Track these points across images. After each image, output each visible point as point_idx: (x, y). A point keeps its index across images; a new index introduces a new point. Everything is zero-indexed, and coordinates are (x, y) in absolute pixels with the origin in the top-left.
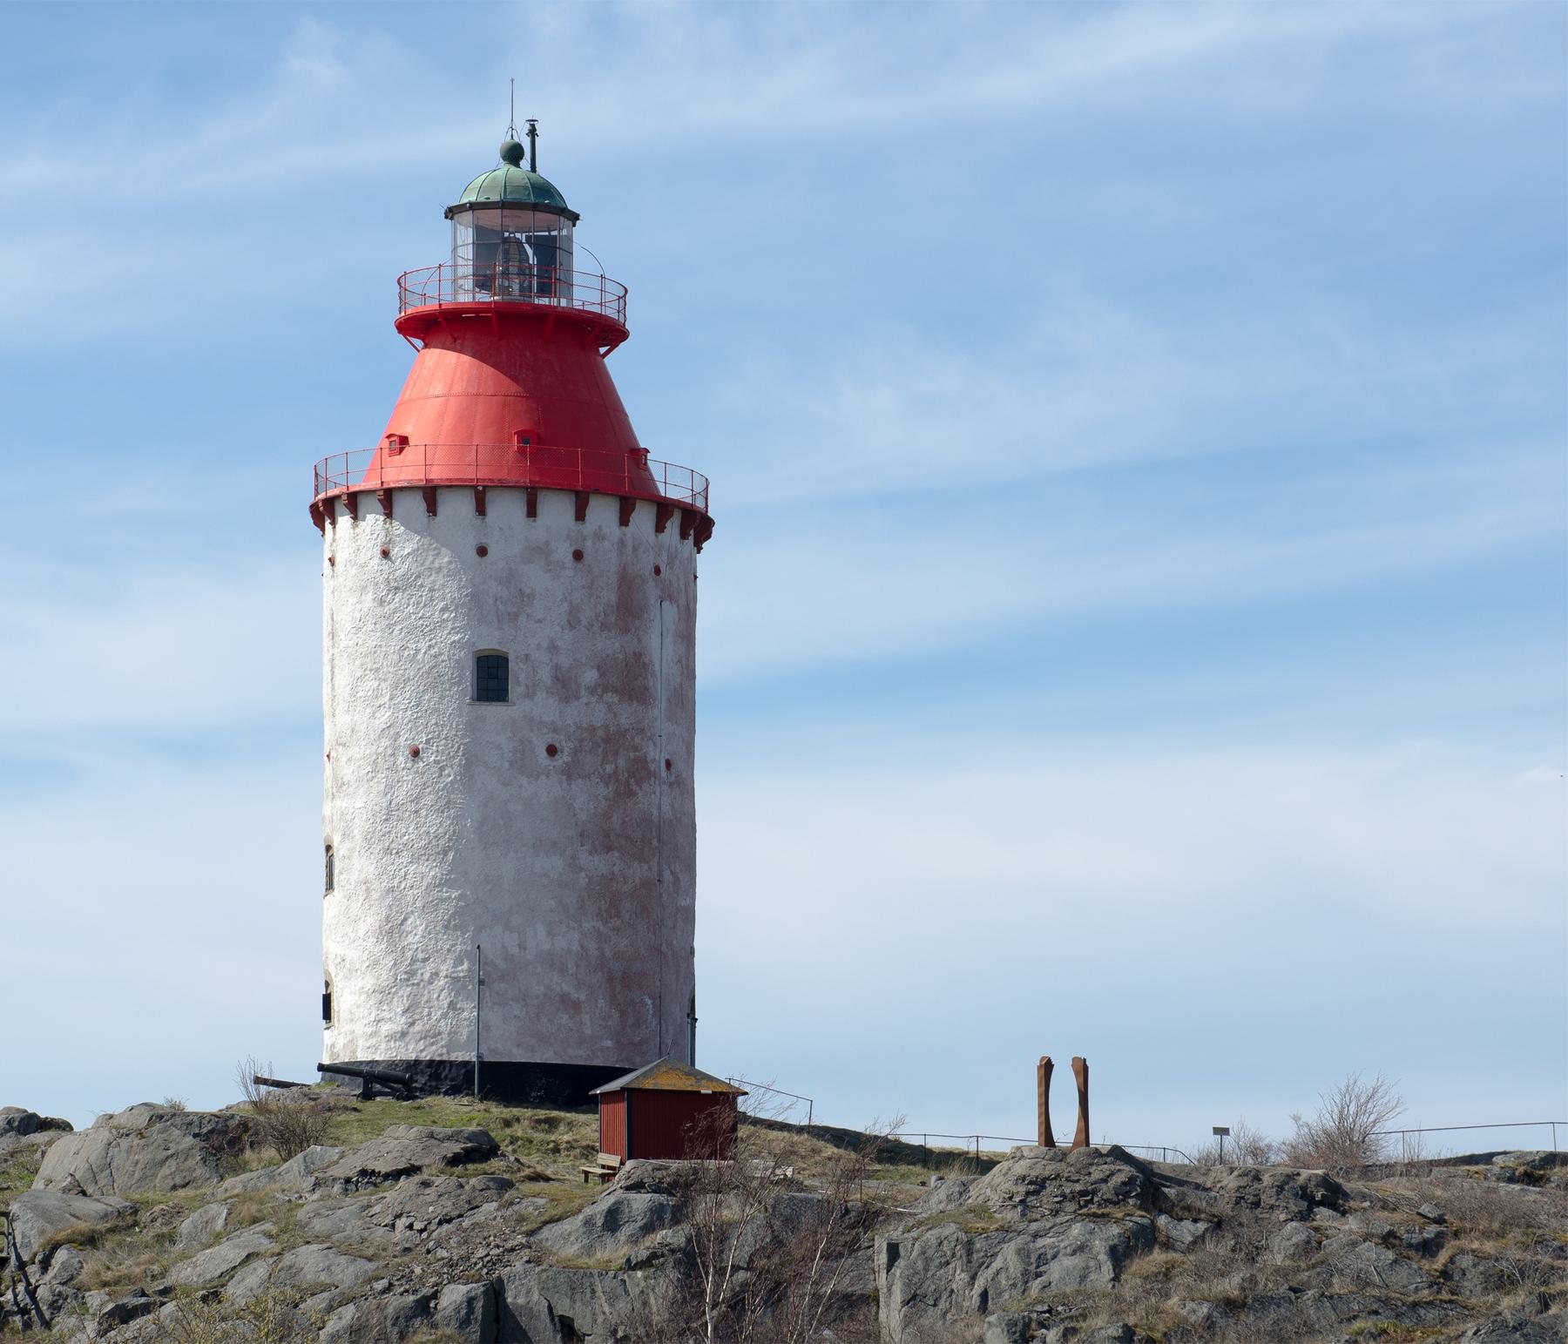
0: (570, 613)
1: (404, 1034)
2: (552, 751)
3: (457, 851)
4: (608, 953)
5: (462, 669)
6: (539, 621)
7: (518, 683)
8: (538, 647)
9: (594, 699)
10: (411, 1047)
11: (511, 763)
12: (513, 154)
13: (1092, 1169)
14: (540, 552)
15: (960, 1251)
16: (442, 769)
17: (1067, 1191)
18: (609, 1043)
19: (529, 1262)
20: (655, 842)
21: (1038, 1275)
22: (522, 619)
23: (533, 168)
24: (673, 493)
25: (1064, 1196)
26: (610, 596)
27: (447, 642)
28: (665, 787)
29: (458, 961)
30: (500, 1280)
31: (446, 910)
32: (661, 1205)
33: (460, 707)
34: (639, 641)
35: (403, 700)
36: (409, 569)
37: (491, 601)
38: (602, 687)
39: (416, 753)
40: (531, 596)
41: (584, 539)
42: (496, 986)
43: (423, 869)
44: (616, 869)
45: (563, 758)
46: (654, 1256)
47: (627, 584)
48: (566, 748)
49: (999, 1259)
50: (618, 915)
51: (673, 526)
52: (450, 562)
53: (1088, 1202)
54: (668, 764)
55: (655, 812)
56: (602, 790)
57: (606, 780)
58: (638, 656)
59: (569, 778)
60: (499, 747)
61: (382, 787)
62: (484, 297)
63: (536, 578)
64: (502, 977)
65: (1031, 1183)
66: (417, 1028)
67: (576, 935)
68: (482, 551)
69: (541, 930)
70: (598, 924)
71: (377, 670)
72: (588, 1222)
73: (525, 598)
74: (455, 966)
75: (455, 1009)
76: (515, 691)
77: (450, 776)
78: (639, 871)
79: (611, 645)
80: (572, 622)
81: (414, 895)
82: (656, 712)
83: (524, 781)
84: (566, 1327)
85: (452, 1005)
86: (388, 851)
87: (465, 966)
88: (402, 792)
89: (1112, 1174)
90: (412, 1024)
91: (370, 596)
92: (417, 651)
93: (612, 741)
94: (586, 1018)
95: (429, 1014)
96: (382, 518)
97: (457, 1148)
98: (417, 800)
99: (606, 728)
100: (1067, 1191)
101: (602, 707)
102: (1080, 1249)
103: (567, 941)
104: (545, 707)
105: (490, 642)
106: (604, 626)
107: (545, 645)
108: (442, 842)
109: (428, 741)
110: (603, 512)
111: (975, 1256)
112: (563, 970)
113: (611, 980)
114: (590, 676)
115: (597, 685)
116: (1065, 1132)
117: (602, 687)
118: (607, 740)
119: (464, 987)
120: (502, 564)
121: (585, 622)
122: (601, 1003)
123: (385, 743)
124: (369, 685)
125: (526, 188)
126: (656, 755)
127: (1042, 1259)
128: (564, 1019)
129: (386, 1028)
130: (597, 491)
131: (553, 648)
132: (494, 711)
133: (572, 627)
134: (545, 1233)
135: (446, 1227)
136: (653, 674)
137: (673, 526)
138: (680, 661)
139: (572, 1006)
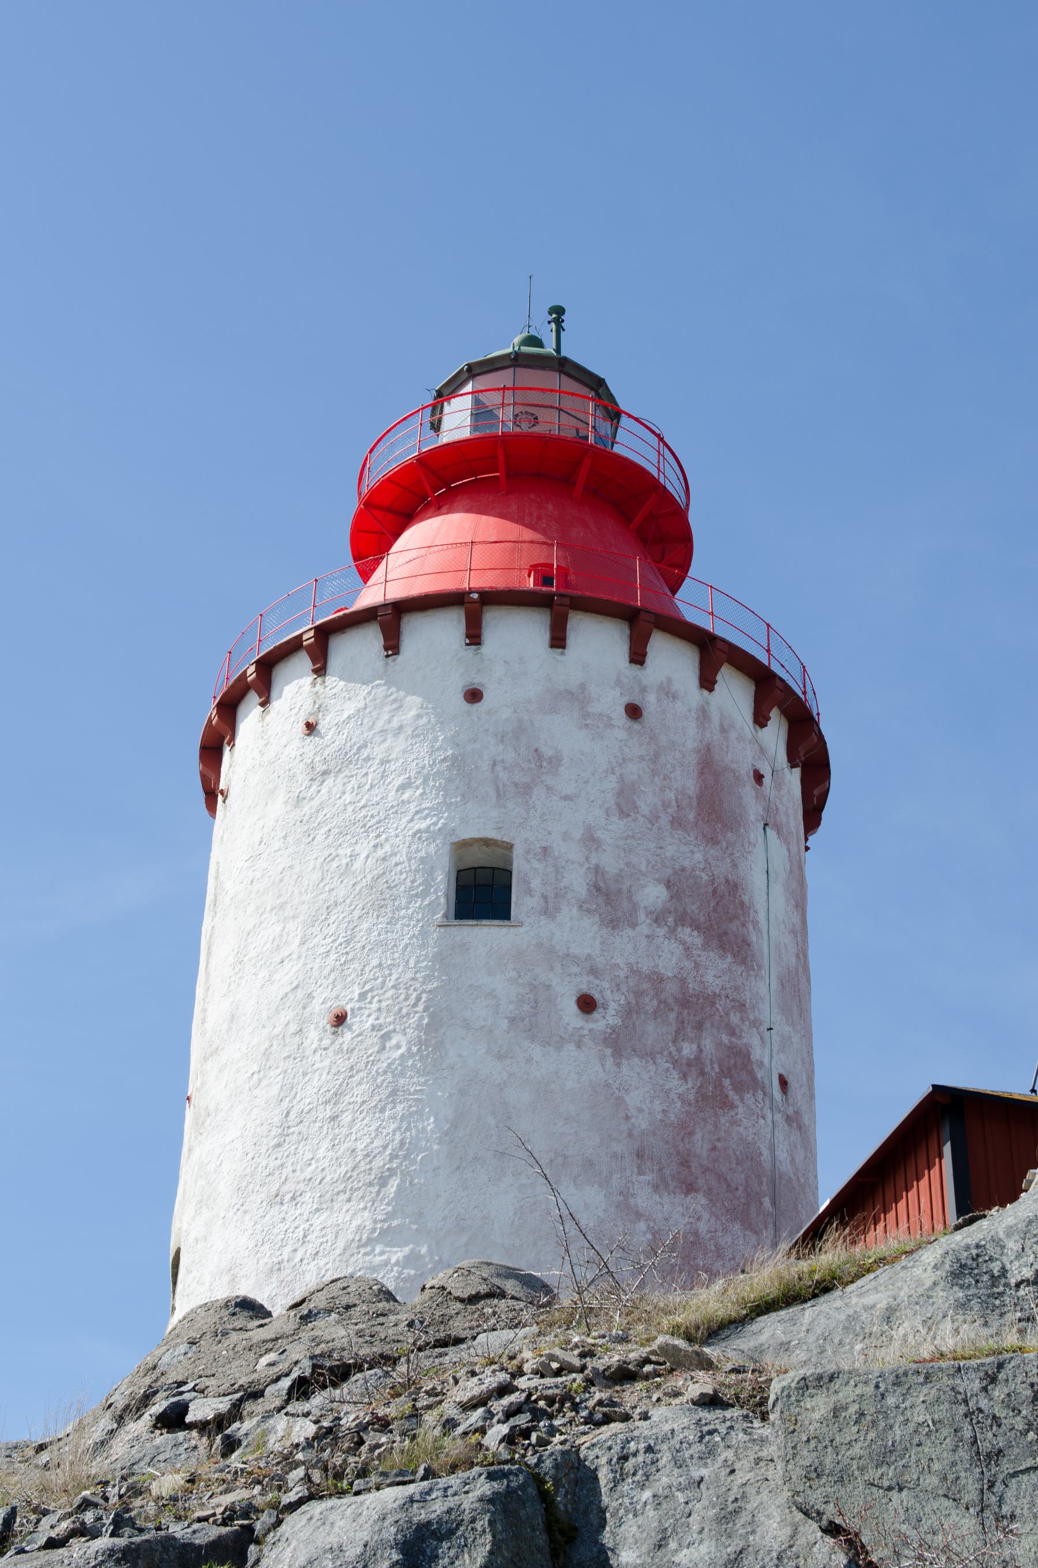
0: (620, 793)
2: (587, 1004)
5: (430, 872)
6: (567, 798)
7: (529, 892)
8: (566, 836)
9: (661, 932)
11: (513, 1020)
14: (577, 698)
16: (386, 1037)
22: (539, 794)
30: (577, 1473)
33: (424, 934)
34: (735, 866)
36: (349, 738)
37: (485, 765)
38: (674, 916)
39: (340, 1019)
40: (555, 761)
41: (643, 690)
43: (342, 1218)
44: (702, 1227)
52: (419, 716)
54: (784, 1083)
56: (675, 1083)
58: (734, 887)
59: (618, 1053)
60: (492, 995)
61: (275, 1090)
63: (562, 734)
68: (474, 696)
71: (282, 906)
73: (543, 762)
76: (520, 902)
77: (400, 1044)
79: (688, 853)
80: (625, 802)
83: (536, 1051)
86: (277, 1199)
88: (309, 1093)
92: (353, 857)
93: (692, 1008)
99: (683, 981)
101: (678, 950)
104: (578, 932)
105: (481, 825)
106: (677, 822)
107: (577, 834)
108: (379, 1162)
109: (363, 996)
114: (653, 894)
115: (666, 912)
117: (674, 916)
118: (685, 1002)
120: (506, 714)
121: (645, 810)
126: (769, 1058)
132: (484, 934)
133: (623, 814)
136: (755, 924)
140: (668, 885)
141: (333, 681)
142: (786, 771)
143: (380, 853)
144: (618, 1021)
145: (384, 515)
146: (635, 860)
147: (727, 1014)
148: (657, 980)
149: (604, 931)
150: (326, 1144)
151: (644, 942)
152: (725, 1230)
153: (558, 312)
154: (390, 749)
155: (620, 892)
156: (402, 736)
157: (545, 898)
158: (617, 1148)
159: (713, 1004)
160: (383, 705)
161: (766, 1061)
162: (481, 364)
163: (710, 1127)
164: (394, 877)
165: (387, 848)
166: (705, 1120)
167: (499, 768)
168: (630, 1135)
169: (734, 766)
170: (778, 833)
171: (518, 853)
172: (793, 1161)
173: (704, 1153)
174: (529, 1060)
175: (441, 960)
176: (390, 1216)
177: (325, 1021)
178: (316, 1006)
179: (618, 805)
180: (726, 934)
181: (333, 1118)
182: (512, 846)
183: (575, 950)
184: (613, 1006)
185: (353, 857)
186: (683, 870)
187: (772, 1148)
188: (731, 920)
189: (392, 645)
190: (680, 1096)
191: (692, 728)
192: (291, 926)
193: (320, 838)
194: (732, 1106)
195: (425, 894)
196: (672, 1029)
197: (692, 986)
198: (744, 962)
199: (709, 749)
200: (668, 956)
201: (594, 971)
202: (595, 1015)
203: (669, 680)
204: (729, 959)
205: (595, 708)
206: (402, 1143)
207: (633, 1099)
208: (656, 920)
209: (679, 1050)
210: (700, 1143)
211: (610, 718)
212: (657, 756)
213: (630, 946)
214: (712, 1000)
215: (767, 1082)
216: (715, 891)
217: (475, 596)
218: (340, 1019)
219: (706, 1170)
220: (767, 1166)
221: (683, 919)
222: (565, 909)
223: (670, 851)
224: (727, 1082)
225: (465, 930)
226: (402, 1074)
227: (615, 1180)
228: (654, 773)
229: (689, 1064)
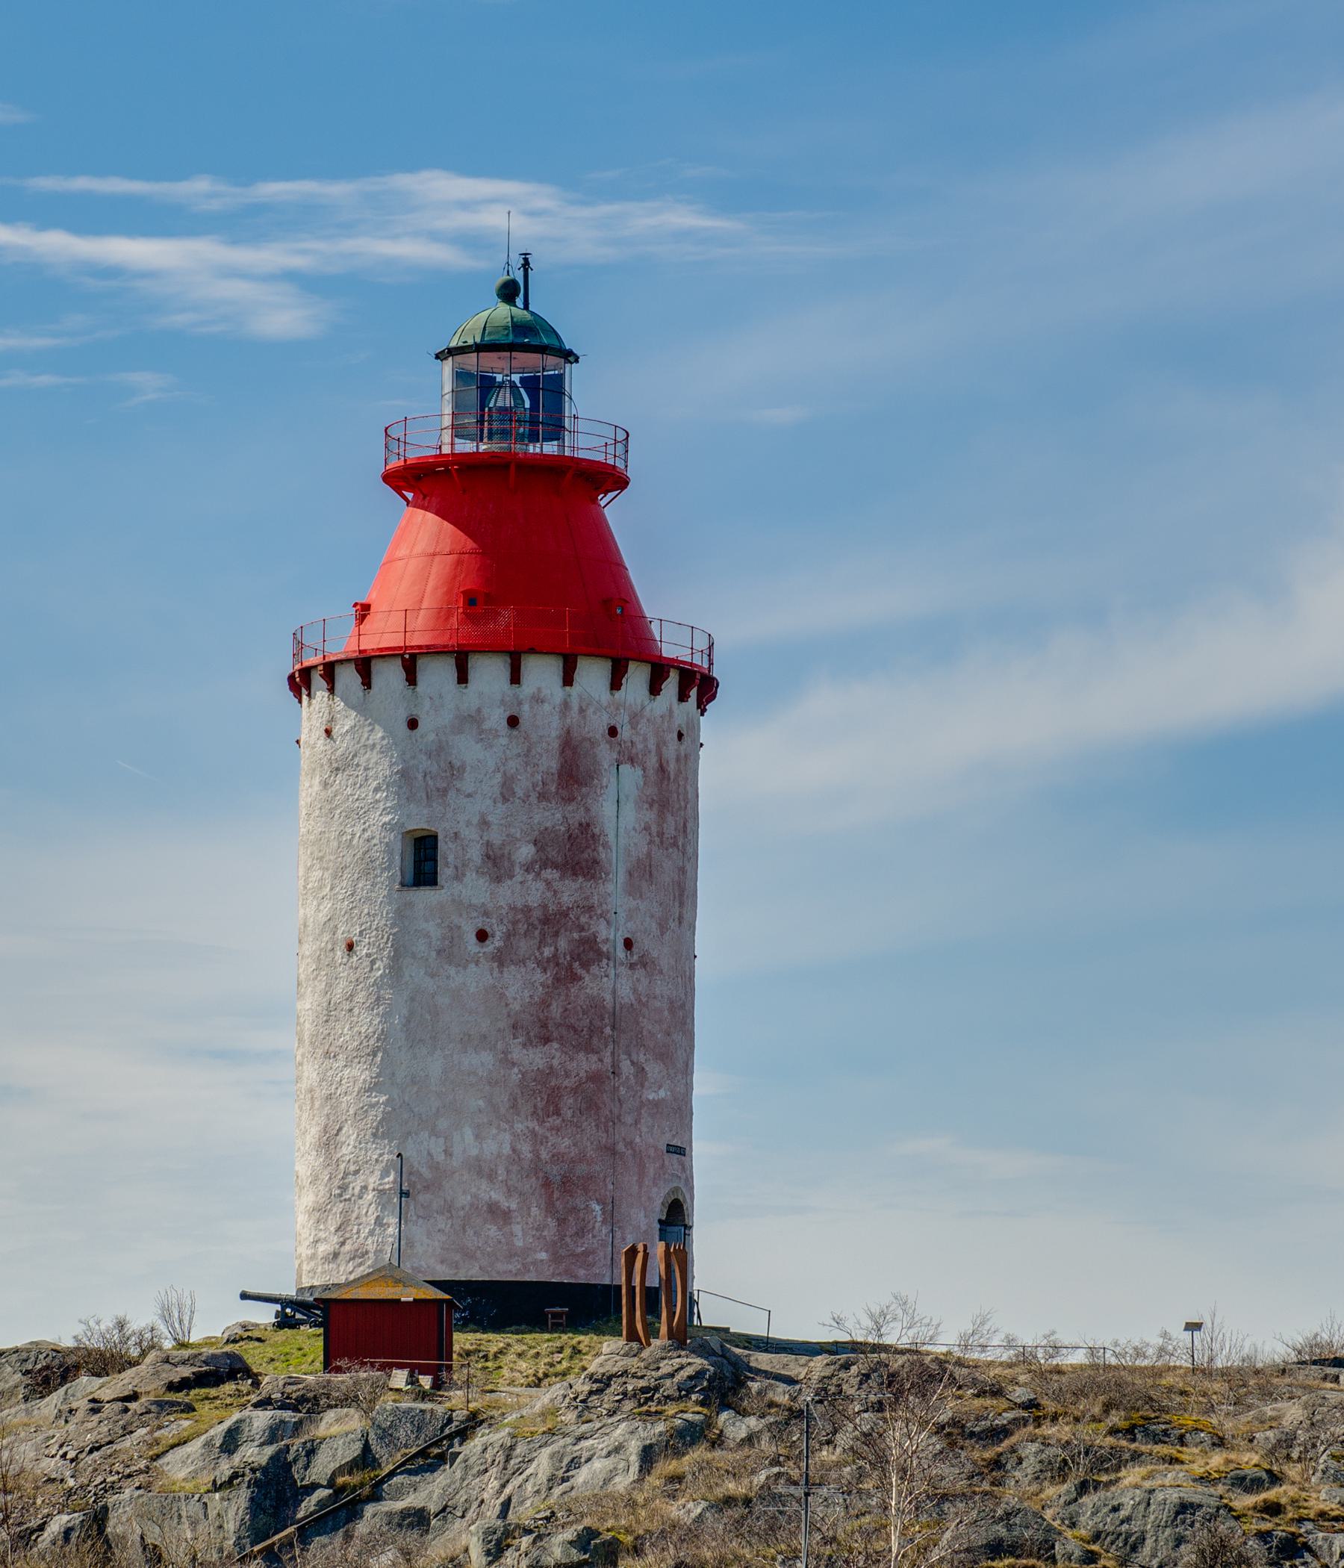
0: (504, 784)
1: (336, 1255)
2: (482, 936)
3: (385, 1052)
4: (544, 1155)
6: (469, 796)
7: (447, 865)
8: (468, 823)
9: (530, 877)
10: (342, 1269)
11: (439, 952)
12: (509, 292)
14: (472, 720)
15: (501, 1458)
16: (373, 963)
17: (630, 1388)
18: (543, 1256)
19: (139, 1488)
20: (608, 1030)
21: (564, 1480)
22: (452, 794)
23: (526, 307)
24: (668, 652)
25: (625, 1394)
26: (550, 763)
27: (379, 824)
28: (622, 970)
29: (385, 1173)
31: (377, 1114)
32: (282, 1422)
33: (389, 896)
34: (588, 810)
35: (344, 885)
37: (420, 777)
38: (541, 863)
39: (350, 947)
41: (520, 703)
42: (421, 1198)
43: (356, 1072)
44: (555, 1062)
45: (495, 943)
46: (235, 1476)
48: (498, 932)
49: (534, 1464)
50: (557, 1113)
51: (671, 686)
52: (383, 738)
53: (647, 1400)
54: (628, 944)
55: (608, 997)
56: (539, 977)
57: (543, 965)
58: (585, 827)
60: (427, 936)
62: (466, 447)
64: (427, 1188)
65: (596, 1381)
66: (347, 1247)
67: (507, 1137)
68: (413, 724)
69: (468, 1133)
70: (533, 1124)
71: (321, 859)
72: (208, 1444)
73: (454, 771)
74: (382, 1178)
75: (381, 1225)
76: (444, 873)
78: (584, 1064)
80: (506, 794)
81: (348, 1103)
82: (610, 887)
83: (452, 971)
84: (154, 1555)
85: (379, 1221)
87: (391, 1178)
88: (340, 989)
89: (682, 1368)
90: (343, 1244)
91: (317, 780)
92: (353, 835)
93: (551, 921)
94: (517, 1229)
95: (358, 1232)
96: (327, 694)
97: (186, 1372)
98: (350, 998)
99: (545, 907)
101: (541, 885)
102: (617, 1449)
103: (497, 1144)
105: (419, 822)
106: (543, 797)
107: (475, 821)
108: (372, 1042)
109: (361, 932)
110: (593, 674)
111: (512, 1462)
112: (491, 1177)
113: (547, 1184)
114: (525, 852)
115: (533, 862)
117: (541, 863)
118: (546, 921)
119: (390, 1200)
120: (432, 737)
121: (520, 793)
122: (534, 1211)
123: (326, 937)
124: (317, 874)
125: (506, 328)
127: (575, 1463)
128: (493, 1231)
129: (323, 1249)
130: (533, 651)
131: (484, 824)
132: (425, 896)
133: (505, 800)
134: (169, 1457)
135: (96, 1454)
136: (606, 845)
137: (671, 686)
138: (647, 828)
139: (497, 1213)
143: (366, 835)
144: (502, 944)
146: (513, 831)
148: (527, 910)
151: (519, 886)
152: (572, 1059)
154: (369, 760)
155: (503, 855)
157: (456, 868)
158: (501, 1025)
161: (612, 937)
163: (563, 998)
164: (374, 854)
166: (559, 994)
172: (635, 990)
174: (448, 978)
176: (378, 1075)
178: (339, 935)
181: (350, 1010)
182: (435, 837)
183: (474, 901)
184: (498, 934)
187: (614, 992)
190: (542, 984)
194: (581, 978)
196: (537, 941)
197: (552, 908)
198: (593, 877)
199: (568, 732)
203: (539, 690)
204: (581, 879)
205: (486, 726)
207: (510, 993)
208: (527, 870)
209: (542, 954)
212: (529, 751)
214: (565, 914)
215: (612, 950)
218: (350, 947)
219: (558, 1025)
221: (546, 864)
223: (537, 818)
225: (411, 893)
227: (499, 1046)
228: (527, 764)
229: (548, 960)
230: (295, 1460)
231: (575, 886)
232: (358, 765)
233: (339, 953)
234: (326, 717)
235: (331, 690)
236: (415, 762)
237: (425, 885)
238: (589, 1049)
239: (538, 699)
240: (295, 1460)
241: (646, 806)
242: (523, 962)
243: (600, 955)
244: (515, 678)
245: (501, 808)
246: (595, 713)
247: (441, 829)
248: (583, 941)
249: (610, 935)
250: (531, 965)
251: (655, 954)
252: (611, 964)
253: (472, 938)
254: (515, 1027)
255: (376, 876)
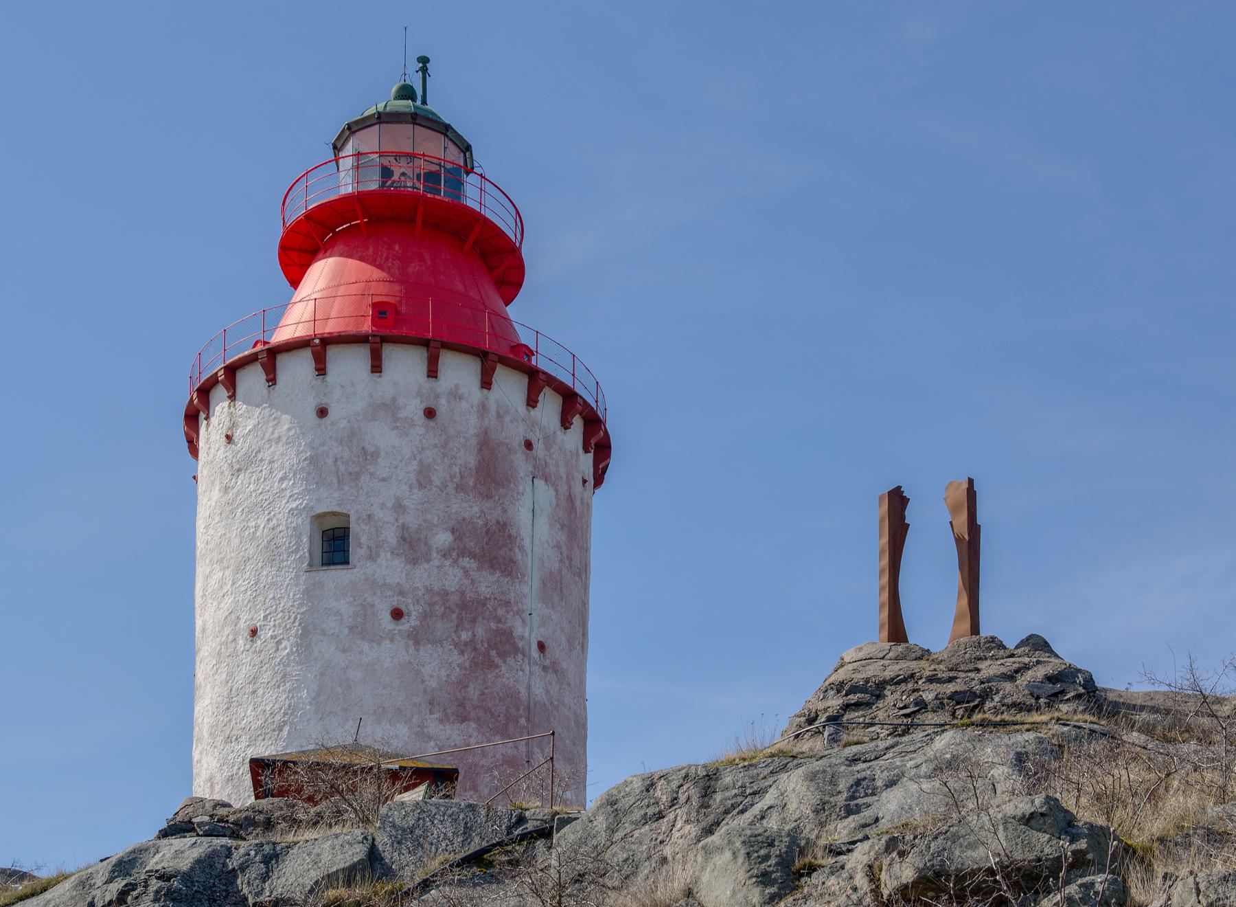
0: (420, 473)
2: (397, 614)
6: (383, 480)
7: (360, 545)
8: (383, 506)
9: (447, 563)
11: (351, 628)
13: (982, 665)
14: (389, 408)
15: (692, 791)
16: (279, 643)
20: (523, 721)
22: (365, 478)
26: (470, 459)
28: (535, 668)
33: (297, 576)
34: (505, 511)
37: (330, 462)
38: (458, 551)
39: (254, 632)
40: (376, 455)
41: (437, 396)
47: (488, 447)
52: (289, 429)
54: (541, 647)
56: (455, 658)
57: (462, 648)
58: (503, 526)
59: (417, 643)
60: (338, 613)
63: (381, 435)
68: (322, 412)
71: (222, 560)
73: (368, 456)
79: (470, 508)
80: (423, 479)
83: (365, 646)
86: (228, 740)
88: (241, 678)
89: (1026, 667)
92: (257, 527)
93: (468, 608)
99: (462, 593)
100: (928, 696)
101: (458, 573)
104: (391, 569)
105: (329, 503)
106: (460, 488)
107: (390, 504)
108: (278, 717)
109: (265, 617)
111: (718, 797)
114: (443, 538)
115: (451, 549)
116: (935, 627)
117: (458, 551)
118: (463, 606)
120: (343, 424)
121: (437, 482)
123: (227, 631)
131: (399, 507)
132: (336, 576)
133: (421, 486)
136: (521, 548)
140: (453, 531)
141: (241, 406)
142: (559, 433)
143: (271, 524)
145: (297, 252)
146: (429, 517)
147: (495, 610)
148: (444, 594)
149: (408, 567)
150: (251, 708)
151: (436, 571)
153: (424, 60)
154: (274, 453)
155: (419, 540)
156: (281, 444)
157: (369, 548)
159: (484, 605)
160: (268, 422)
161: (527, 635)
162: (356, 122)
164: (279, 541)
165: (275, 521)
166: (476, 678)
167: (339, 463)
168: (425, 692)
169: (507, 441)
170: (546, 481)
171: (353, 519)
172: (547, 692)
173: (476, 698)
174: (361, 652)
175: (308, 593)
177: (246, 634)
178: (242, 624)
179: (418, 481)
180: (495, 558)
181: (254, 692)
185: (257, 527)
186: (464, 519)
187: (529, 687)
188: (500, 549)
189: (272, 379)
190: (459, 665)
191: (473, 420)
192: (227, 573)
193: (238, 514)
194: (497, 666)
195: (297, 551)
198: (510, 574)
200: (453, 578)
201: (402, 593)
202: (403, 620)
203: (457, 386)
204: (498, 573)
205: (403, 414)
206: (290, 706)
207: (427, 670)
208: (444, 556)
209: (459, 637)
210: (473, 692)
211: (412, 420)
212: (446, 443)
213: (425, 575)
214: (483, 603)
215: (527, 648)
216: (487, 531)
217: (317, 341)
218: (254, 632)
219: (476, 707)
220: (524, 698)
221: (463, 552)
222: (383, 555)
223: (455, 508)
224: (493, 653)
225: (321, 573)
226: (288, 665)
228: (444, 455)
229: (466, 644)
230: (243, 868)
231: (493, 579)
232: (261, 460)
233: (241, 642)
234: (227, 424)
235: (232, 397)
236: (326, 448)
237: (334, 564)
238: (505, 734)
239: (455, 395)
240: (243, 868)
241: (558, 526)
242: (440, 642)
243: (516, 650)
244: (433, 373)
245: (417, 495)
246: (512, 421)
247: (355, 513)
248: (499, 633)
249: (527, 632)
250: (448, 646)
251: (564, 665)
252: (526, 661)
253: (386, 617)
254: (431, 703)
255: (282, 561)
